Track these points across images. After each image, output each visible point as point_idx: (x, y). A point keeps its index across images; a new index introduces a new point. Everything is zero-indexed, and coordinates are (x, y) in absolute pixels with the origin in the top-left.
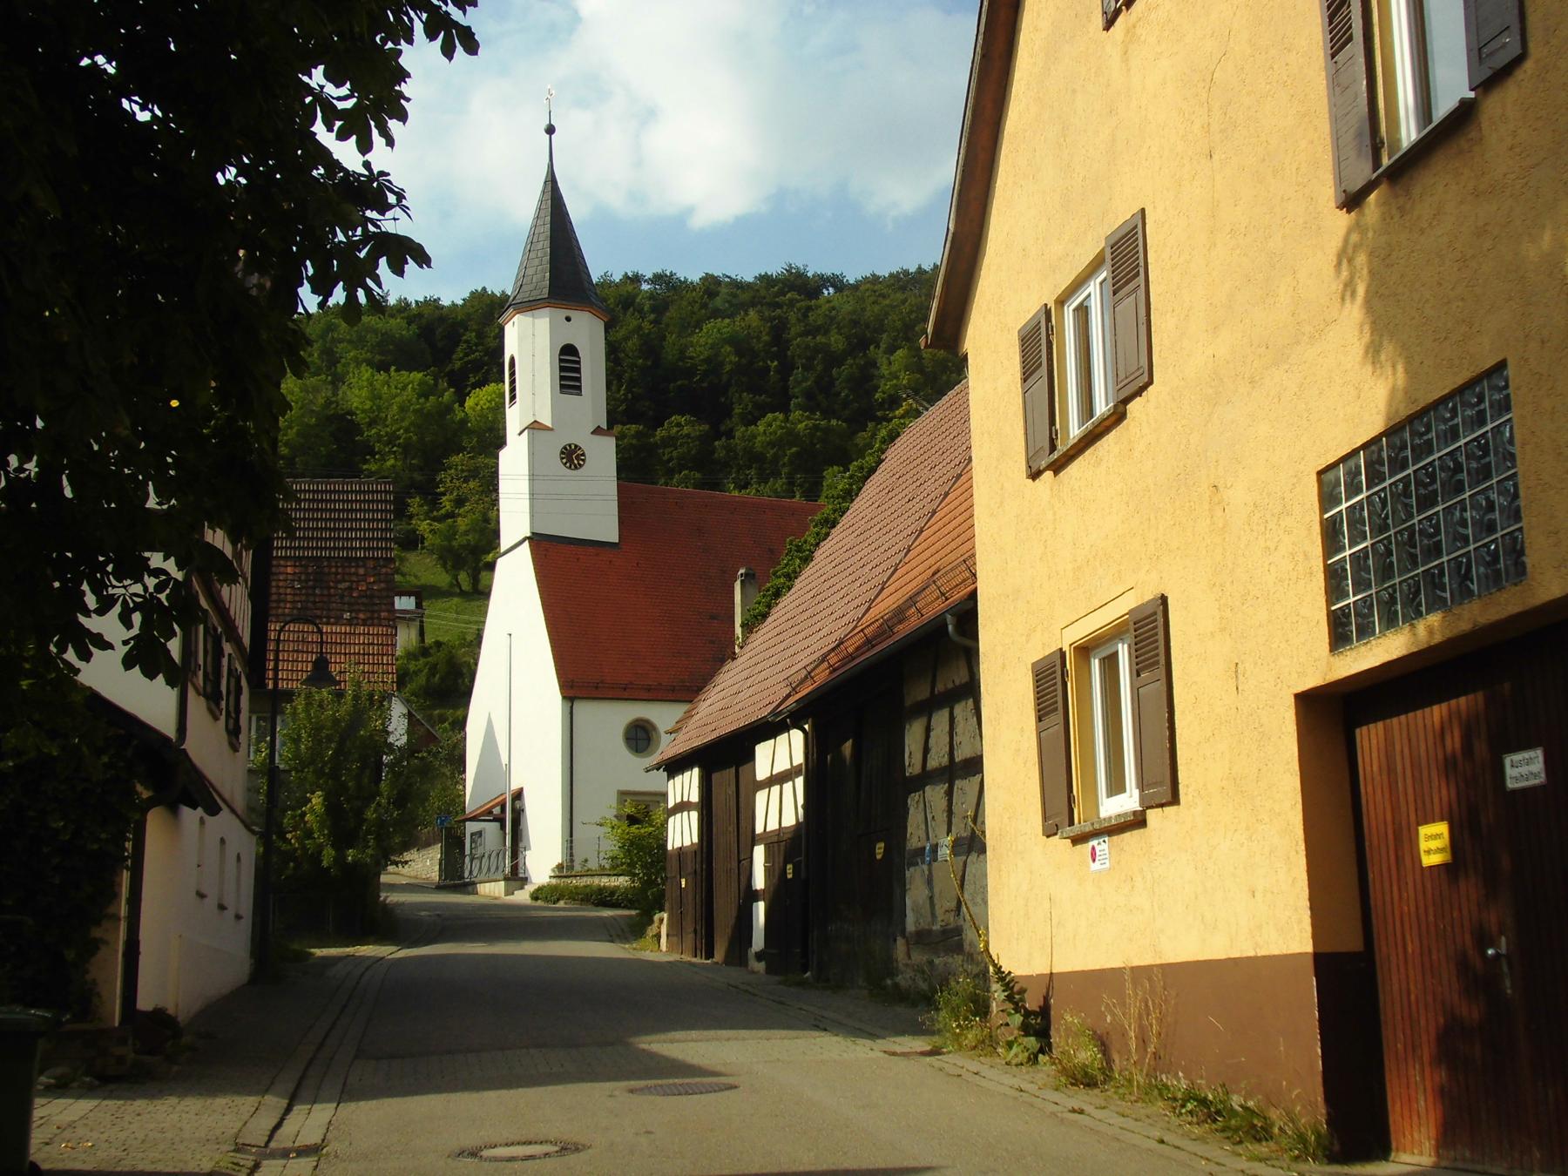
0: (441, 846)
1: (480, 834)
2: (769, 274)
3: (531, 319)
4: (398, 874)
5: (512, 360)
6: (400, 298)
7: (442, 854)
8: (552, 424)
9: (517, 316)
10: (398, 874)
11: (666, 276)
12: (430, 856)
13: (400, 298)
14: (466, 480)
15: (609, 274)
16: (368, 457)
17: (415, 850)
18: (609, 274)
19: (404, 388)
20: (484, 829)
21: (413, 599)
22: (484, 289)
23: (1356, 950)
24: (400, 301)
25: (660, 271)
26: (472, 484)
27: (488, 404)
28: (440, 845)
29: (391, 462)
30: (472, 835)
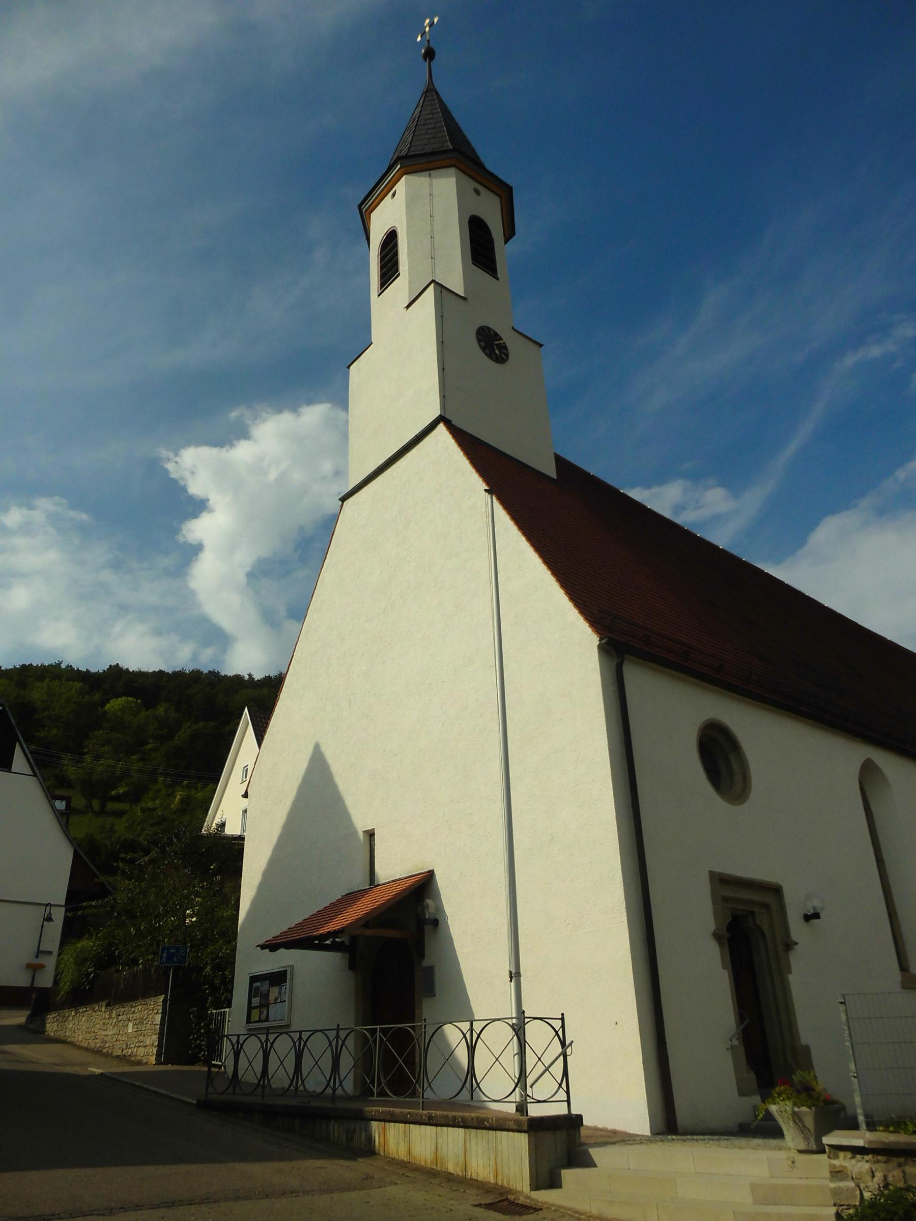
0: (164, 1001)
1: (279, 978)
2: (271, 676)
3: (428, 179)
4: (64, 1042)
5: (391, 238)
6: (68, 666)
7: (163, 1013)
8: (465, 292)
9: (404, 177)
10: (64, 1042)
11: (215, 672)
12: (137, 1015)
13: (68, 666)
14: (103, 745)
15: (185, 669)
16: (40, 728)
17: (104, 1004)
18: (185, 669)
19: (70, 689)
20: (292, 966)
21: (64, 803)
22: (118, 664)
23: (26, 986)
24: (68, 666)
25: (212, 670)
26: (107, 748)
27: (118, 707)
28: (162, 998)
29: (55, 731)
30: (253, 979)
